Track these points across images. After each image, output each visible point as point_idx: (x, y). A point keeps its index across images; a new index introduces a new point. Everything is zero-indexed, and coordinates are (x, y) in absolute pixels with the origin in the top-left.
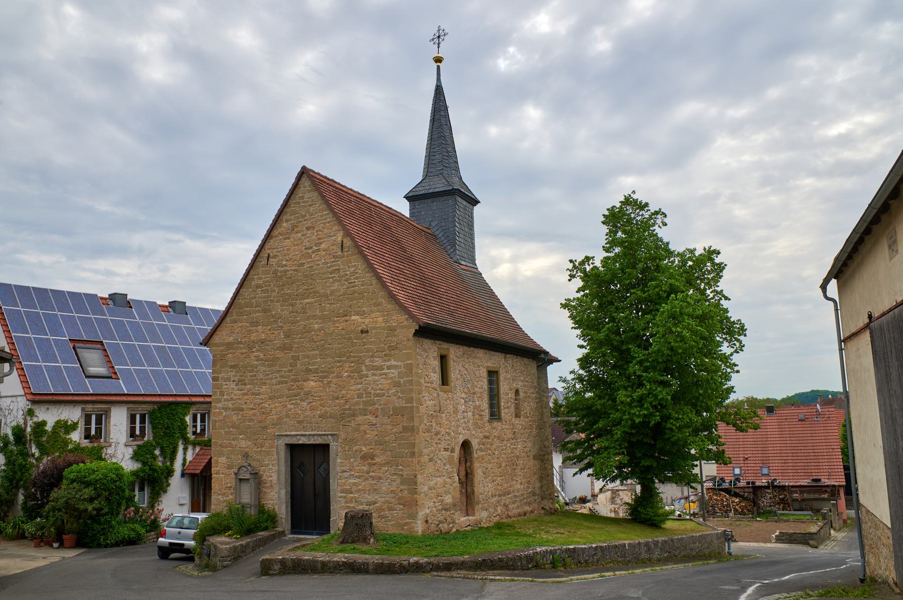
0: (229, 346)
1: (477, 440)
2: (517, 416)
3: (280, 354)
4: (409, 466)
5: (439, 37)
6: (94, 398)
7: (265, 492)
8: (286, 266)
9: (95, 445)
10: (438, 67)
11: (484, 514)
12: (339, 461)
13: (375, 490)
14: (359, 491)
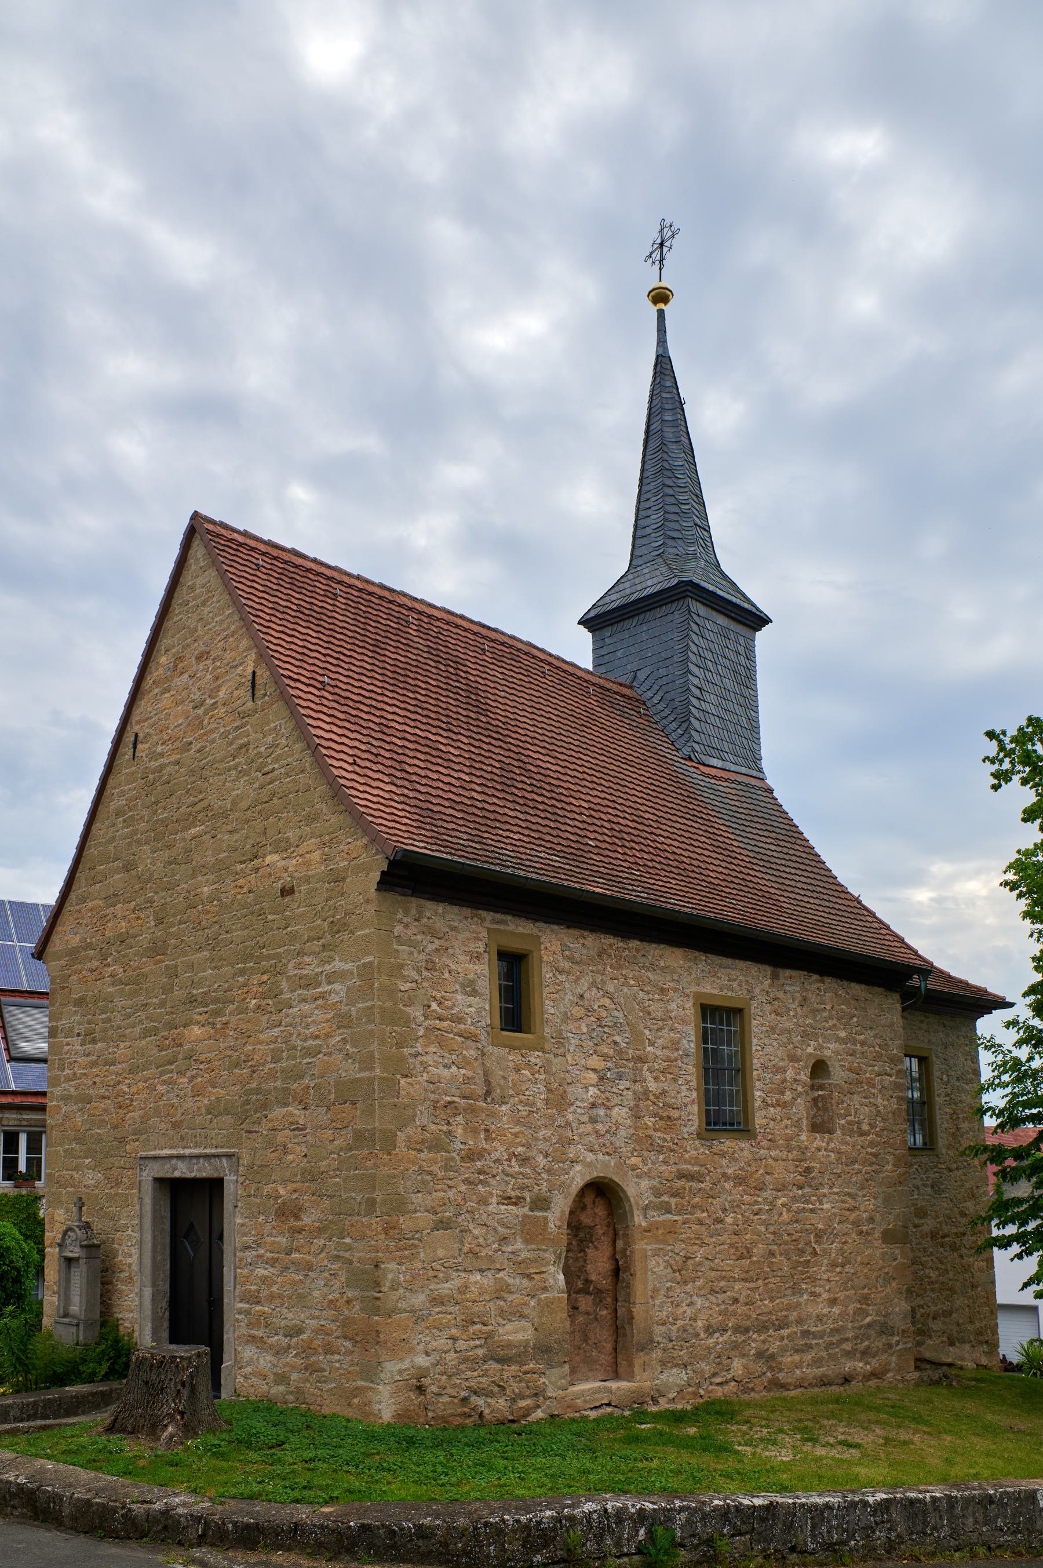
0: (73, 954)
1: (645, 1183)
2: (817, 1128)
3: (148, 967)
4: (363, 1237)
5: (662, 244)
6: (17, 1100)
7: (121, 1291)
8: (162, 755)
9: (24, 1192)
10: (661, 314)
11: (675, 1377)
12: (239, 1221)
13: (301, 1297)
14: (272, 1297)
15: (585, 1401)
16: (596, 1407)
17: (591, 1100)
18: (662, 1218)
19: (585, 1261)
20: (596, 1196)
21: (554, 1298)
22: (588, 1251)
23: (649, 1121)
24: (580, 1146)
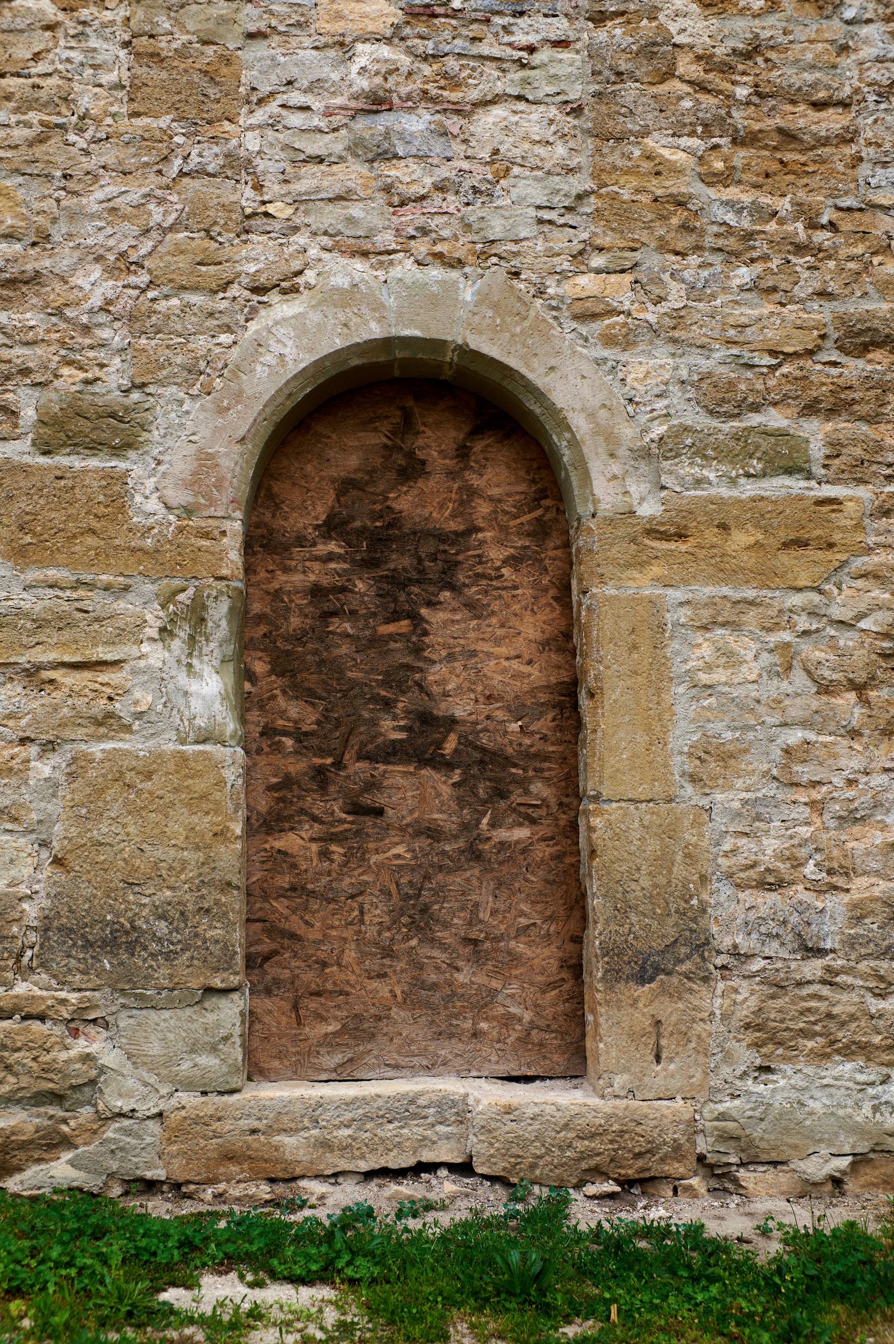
15: (326, 1145)
16: (384, 1173)
17: (363, 84)
18: (749, 489)
19: (417, 650)
20: (475, 432)
21: (158, 756)
22: (435, 617)
23: (677, 151)
24: (301, 239)
